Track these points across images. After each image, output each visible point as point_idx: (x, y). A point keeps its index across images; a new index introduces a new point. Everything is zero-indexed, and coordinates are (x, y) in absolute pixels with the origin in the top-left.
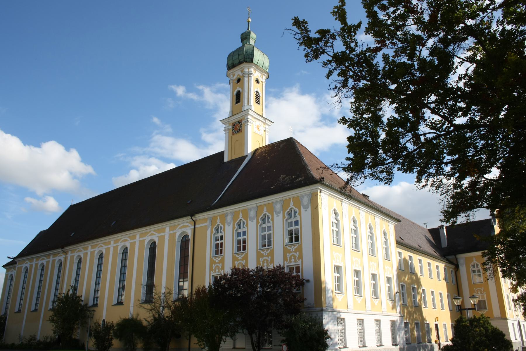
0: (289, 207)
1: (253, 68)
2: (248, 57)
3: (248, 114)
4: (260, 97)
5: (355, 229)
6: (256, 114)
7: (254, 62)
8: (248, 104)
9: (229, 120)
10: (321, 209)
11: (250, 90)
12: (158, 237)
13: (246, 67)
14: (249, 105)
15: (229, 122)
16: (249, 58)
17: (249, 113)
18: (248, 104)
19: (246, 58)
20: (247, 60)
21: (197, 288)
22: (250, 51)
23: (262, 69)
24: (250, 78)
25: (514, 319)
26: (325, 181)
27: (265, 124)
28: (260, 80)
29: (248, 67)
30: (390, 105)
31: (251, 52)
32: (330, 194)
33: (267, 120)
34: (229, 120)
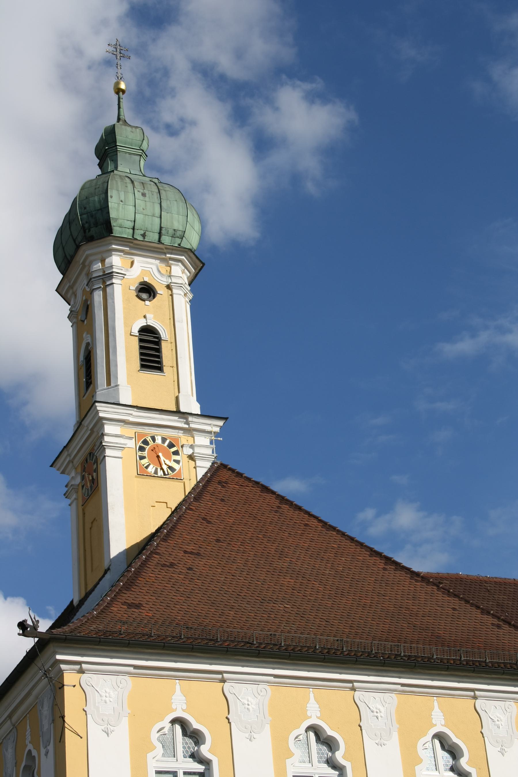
0: (346, 744)
1: (114, 254)
4: (164, 345)
6: (135, 412)
7: (117, 231)
8: (109, 383)
9: (69, 455)
11: (110, 332)
12: (435, 725)
13: (91, 258)
14: (112, 385)
15: (72, 461)
16: (96, 225)
17: (101, 415)
18: (109, 383)
19: (87, 226)
20: (93, 231)
23: (135, 242)
24: (108, 289)
26: (60, 715)
27: (189, 431)
29: (99, 256)
30: (141, 235)
34: (69, 455)
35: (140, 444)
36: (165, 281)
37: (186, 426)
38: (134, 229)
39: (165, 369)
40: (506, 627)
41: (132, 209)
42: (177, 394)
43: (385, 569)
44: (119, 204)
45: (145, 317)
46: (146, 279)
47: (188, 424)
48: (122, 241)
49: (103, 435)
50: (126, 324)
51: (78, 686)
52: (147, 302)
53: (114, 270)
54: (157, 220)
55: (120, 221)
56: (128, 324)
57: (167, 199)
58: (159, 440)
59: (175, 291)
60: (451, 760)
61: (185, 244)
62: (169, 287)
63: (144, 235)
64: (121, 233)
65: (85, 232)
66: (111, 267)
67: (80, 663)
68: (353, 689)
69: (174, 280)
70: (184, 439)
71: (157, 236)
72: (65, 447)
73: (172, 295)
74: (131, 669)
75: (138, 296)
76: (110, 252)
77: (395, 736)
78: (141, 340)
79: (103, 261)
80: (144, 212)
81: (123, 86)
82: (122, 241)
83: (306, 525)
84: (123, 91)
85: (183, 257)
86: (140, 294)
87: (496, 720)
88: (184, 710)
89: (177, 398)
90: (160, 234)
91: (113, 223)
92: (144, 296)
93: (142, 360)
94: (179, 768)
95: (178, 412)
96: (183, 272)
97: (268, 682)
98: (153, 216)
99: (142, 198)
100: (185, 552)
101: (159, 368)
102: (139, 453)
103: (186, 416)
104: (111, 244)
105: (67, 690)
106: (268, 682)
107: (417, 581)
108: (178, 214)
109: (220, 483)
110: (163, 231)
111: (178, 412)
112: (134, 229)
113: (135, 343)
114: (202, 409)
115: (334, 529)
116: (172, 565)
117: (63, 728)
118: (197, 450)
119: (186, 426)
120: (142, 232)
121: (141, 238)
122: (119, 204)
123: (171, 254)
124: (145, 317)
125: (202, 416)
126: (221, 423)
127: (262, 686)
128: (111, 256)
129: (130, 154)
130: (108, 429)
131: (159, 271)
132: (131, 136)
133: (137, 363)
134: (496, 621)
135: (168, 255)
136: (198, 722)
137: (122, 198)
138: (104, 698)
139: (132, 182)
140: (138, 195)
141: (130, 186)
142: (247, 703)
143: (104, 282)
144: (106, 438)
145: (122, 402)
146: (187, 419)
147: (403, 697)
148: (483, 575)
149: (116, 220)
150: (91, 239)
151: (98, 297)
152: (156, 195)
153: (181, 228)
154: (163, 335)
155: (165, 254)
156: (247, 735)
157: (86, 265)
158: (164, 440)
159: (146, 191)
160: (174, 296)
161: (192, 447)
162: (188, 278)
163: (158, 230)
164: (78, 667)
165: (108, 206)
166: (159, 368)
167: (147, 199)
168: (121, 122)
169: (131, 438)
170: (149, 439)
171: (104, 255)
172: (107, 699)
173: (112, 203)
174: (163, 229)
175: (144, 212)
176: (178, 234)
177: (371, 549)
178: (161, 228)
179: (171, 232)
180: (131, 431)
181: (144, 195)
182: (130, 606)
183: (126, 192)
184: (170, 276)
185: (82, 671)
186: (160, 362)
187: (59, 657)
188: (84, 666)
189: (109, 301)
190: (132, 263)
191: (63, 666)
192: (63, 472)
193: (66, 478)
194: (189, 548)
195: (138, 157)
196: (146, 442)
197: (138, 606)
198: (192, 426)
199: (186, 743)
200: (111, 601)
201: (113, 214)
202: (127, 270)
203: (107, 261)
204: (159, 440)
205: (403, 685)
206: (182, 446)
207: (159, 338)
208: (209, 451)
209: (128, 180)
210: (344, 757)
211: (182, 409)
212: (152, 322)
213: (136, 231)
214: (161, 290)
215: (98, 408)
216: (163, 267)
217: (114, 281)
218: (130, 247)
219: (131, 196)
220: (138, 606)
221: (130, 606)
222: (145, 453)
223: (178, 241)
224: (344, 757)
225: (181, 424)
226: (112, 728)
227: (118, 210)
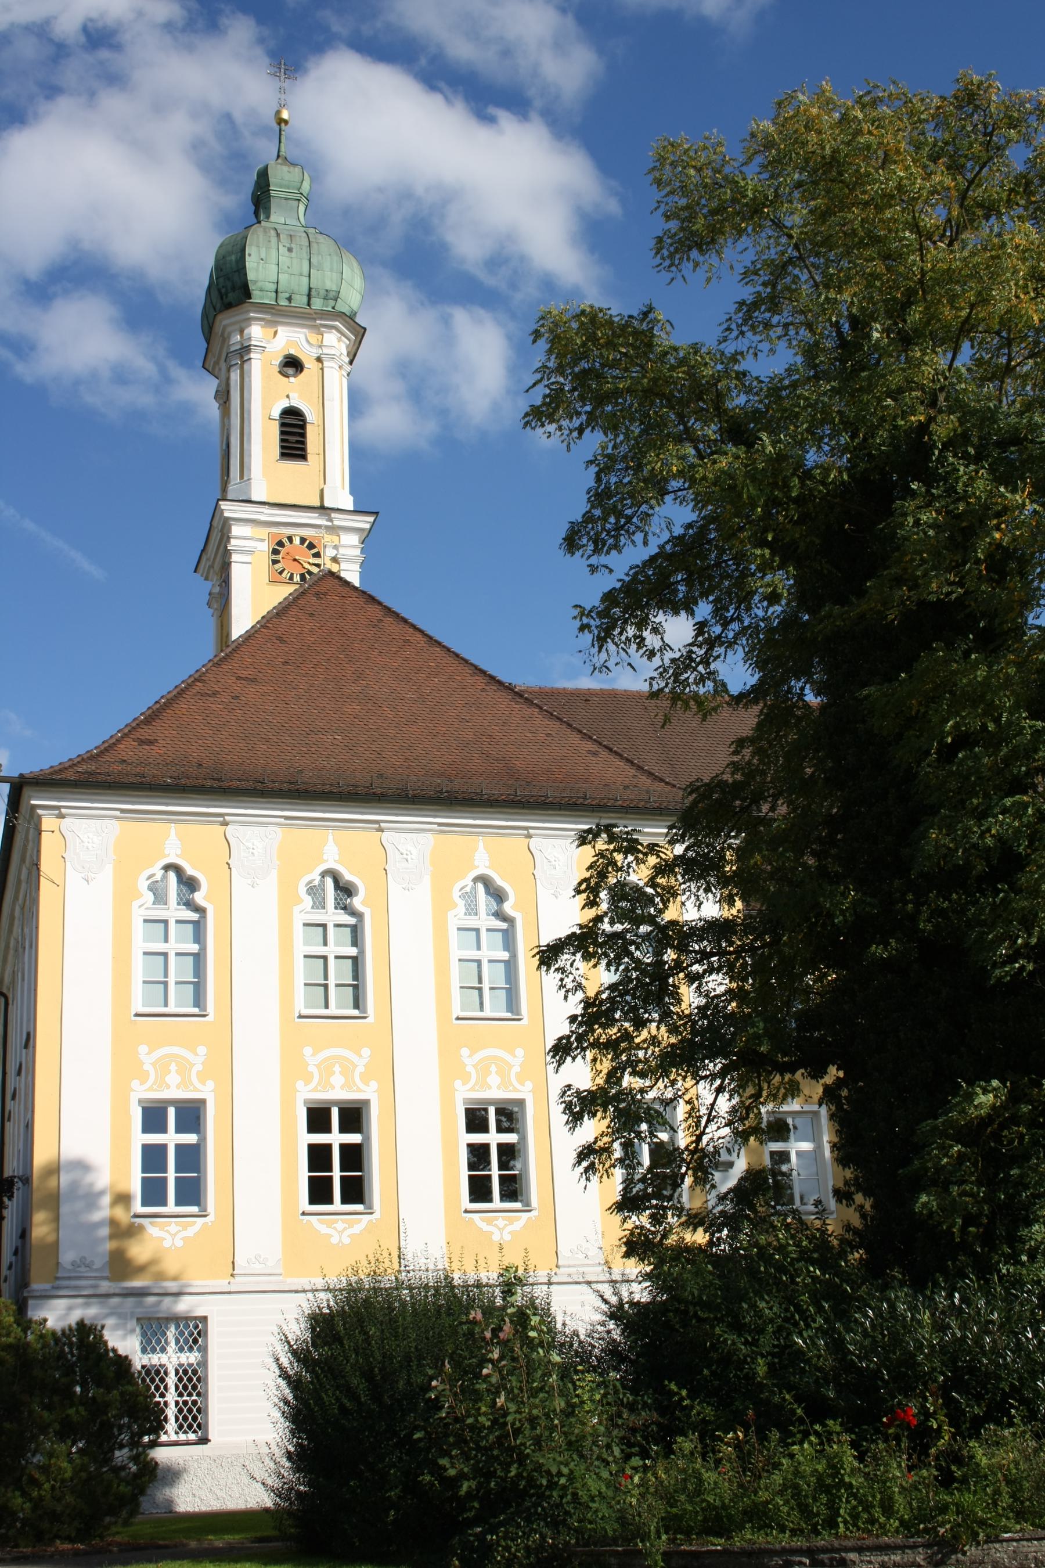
2: (229, 284)
3: (227, 520)
4: (309, 428)
5: (352, 921)
6: (266, 510)
7: (257, 297)
10: (60, 885)
14: (245, 478)
15: (212, 566)
16: (233, 289)
17: (226, 514)
18: (242, 477)
19: (223, 291)
20: (231, 297)
21: (595, 1179)
22: (233, 258)
24: (246, 366)
25: (570, 1280)
28: (307, 355)
29: (237, 327)
31: (237, 262)
32: (122, 811)
33: (333, 515)
35: (273, 546)
36: (315, 352)
37: (329, 524)
38: (277, 292)
39: (309, 457)
40: (604, 754)
41: (274, 268)
42: (322, 486)
43: (483, 690)
44: (258, 263)
45: (288, 396)
46: (292, 352)
47: (332, 521)
48: (263, 307)
49: (229, 538)
50: (264, 407)
51: (57, 832)
52: (292, 379)
53: (253, 343)
54: (305, 280)
55: (259, 284)
56: (266, 406)
57: (319, 254)
58: (297, 541)
59: (326, 364)
60: (495, 904)
61: (341, 307)
62: (319, 359)
63: (289, 299)
64: (262, 298)
65: (222, 298)
66: (250, 339)
67: (58, 808)
68: (381, 830)
69: (325, 351)
70: (328, 539)
71: (305, 299)
72: (203, 551)
73: (322, 369)
74: (118, 813)
75: (280, 372)
76: (248, 321)
77: (427, 880)
78: (282, 425)
79: (242, 332)
80: (290, 270)
81: (285, 115)
82: (263, 307)
83: (407, 641)
84: (286, 122)
85: (337, 323)
86: (285, 369)
87: (552, 860)
88: (177, 856)
89: (322, 491)
90: (309, 296)
91: (251, 287)
92: (290, 371)
93: (282, 447)
94: (171, 917)
95: (322, 509)
96: (339, 340)
97: (277, 824)
98: (301, 275)
99: (287, 253)
100: (239, 678)
101: (303, 457)
102: (274, 557)
103: (328, 511)
104: (249, 311)
105: (44, 836)
106: (277, 824)
107: (517, 703)
108: (331, 270)
109: (317, 594)
110: (313, 293)
111: (322, 509)
112: (277, 292)
113: (275, 429)
114: (355, 503)
115: (439, 644)
116: (215, 694)
117: (39, 875)
118: (342, 551)
119: (329, 524)
120: (287, 295)
121: (286, 303)
122: (258, 263)
123: (321, 319)
124: (288, 396)
125: (355, 512)
126: (371, 519)
127: (270, 828)
128: (250, 325)
129: (286, 199)
130: (236, 530)
131: (308, 341)
132: (287, 177)
133: (277, 451)
134: (595, 747)
135: (318, 322)
136: (194, 867)
137: (263, 256)
138: (86, 844)
139: (278, 235)
140: (283, 250)
141: (274, 240)
142: (251, 846)
143: (242, 357)
144: (233, 542)
145: (254, 499)
146: (329, 515)
147: (442, 836)
148: (37, 769)
149: (255, 282)
150: (229, 306)
151: (235, 376)
152: (305, 250)
153: (334, 288)
154: (309, 417)
155: (315, 319)
156: (249, 881)
157: (225, 339)
158: (303, 540)
159: (293, 246)
160: (325, 370)
161: (336, 547)
162: (347, 347)
163: (305, 291)
164: (57, 812)
165: (245, 267)
166: (303, 457)
167: (293, 255)
168: (280, 161)
169: (263, 540)
170: (285, 540)
171: (243, 325)
172: (90, 846)
173: (250, 263)
174: (313, 291)
175: (290, 270)
176: (332, 295)
177: (476, 667)
178: (310, 289)
179: (322, 293)
180: (264, 532)
181: (290, 250)
182: (142, 742)
183: (268, 248)
184: (320, 347)
185: (62, 816)
186: (304, 450)
187: (33, 802)
188: (63, 811)
189: (246, 379)
190: (276, 333)
191: (40, 812)
192: (206, 579)
193: (208, 585)
194: (244, 673)
195: (296, 203)
196: (280, 544)
197: (150, 742)
198: (336, 523)
199: (182, 891)
200: (122, 737)
201: (251, 276)
202: (268, 342)
203: (246, 332)
204: (297, 541)
205: (440, 824)
206: (325, 547)
207: (304, 421)
208: (358, 552)
209: (273, 233)
210: (363, 903)
211: (327, 504)
212: (296, 402)
213: (280, 294)
214: (309, 364)
215: (223, 507)
216: (314, 338)
217: (252, 355)
218: (273, 314)
219: (274, 253)
220: (150, 742)
221: (142, 742)
222: (279, 557)
223: (332, 303)
224: (363, 903)
225: (323, 522)
226: (93, 876)
227: (257, 270)
